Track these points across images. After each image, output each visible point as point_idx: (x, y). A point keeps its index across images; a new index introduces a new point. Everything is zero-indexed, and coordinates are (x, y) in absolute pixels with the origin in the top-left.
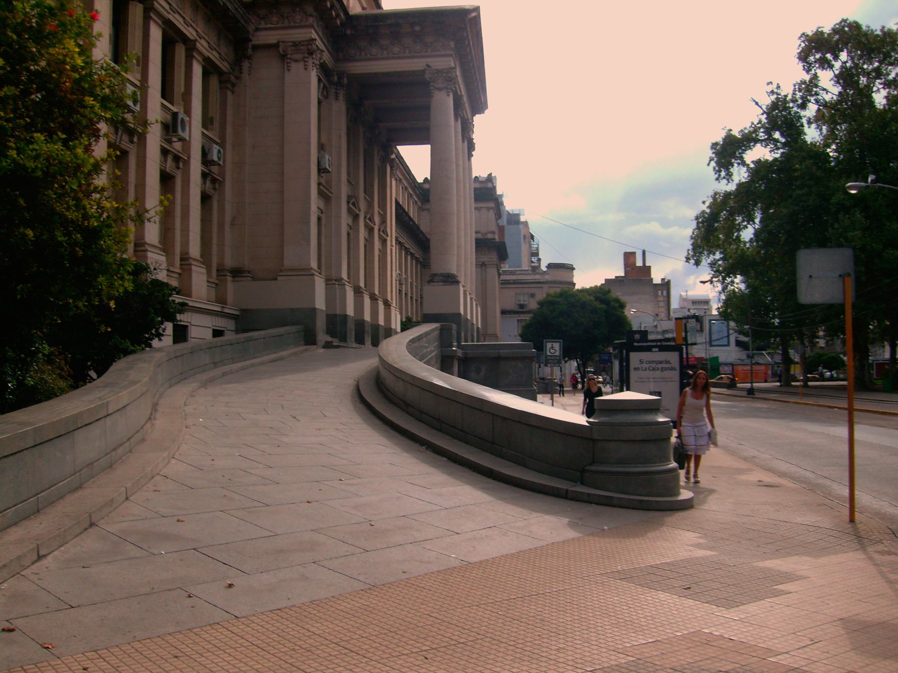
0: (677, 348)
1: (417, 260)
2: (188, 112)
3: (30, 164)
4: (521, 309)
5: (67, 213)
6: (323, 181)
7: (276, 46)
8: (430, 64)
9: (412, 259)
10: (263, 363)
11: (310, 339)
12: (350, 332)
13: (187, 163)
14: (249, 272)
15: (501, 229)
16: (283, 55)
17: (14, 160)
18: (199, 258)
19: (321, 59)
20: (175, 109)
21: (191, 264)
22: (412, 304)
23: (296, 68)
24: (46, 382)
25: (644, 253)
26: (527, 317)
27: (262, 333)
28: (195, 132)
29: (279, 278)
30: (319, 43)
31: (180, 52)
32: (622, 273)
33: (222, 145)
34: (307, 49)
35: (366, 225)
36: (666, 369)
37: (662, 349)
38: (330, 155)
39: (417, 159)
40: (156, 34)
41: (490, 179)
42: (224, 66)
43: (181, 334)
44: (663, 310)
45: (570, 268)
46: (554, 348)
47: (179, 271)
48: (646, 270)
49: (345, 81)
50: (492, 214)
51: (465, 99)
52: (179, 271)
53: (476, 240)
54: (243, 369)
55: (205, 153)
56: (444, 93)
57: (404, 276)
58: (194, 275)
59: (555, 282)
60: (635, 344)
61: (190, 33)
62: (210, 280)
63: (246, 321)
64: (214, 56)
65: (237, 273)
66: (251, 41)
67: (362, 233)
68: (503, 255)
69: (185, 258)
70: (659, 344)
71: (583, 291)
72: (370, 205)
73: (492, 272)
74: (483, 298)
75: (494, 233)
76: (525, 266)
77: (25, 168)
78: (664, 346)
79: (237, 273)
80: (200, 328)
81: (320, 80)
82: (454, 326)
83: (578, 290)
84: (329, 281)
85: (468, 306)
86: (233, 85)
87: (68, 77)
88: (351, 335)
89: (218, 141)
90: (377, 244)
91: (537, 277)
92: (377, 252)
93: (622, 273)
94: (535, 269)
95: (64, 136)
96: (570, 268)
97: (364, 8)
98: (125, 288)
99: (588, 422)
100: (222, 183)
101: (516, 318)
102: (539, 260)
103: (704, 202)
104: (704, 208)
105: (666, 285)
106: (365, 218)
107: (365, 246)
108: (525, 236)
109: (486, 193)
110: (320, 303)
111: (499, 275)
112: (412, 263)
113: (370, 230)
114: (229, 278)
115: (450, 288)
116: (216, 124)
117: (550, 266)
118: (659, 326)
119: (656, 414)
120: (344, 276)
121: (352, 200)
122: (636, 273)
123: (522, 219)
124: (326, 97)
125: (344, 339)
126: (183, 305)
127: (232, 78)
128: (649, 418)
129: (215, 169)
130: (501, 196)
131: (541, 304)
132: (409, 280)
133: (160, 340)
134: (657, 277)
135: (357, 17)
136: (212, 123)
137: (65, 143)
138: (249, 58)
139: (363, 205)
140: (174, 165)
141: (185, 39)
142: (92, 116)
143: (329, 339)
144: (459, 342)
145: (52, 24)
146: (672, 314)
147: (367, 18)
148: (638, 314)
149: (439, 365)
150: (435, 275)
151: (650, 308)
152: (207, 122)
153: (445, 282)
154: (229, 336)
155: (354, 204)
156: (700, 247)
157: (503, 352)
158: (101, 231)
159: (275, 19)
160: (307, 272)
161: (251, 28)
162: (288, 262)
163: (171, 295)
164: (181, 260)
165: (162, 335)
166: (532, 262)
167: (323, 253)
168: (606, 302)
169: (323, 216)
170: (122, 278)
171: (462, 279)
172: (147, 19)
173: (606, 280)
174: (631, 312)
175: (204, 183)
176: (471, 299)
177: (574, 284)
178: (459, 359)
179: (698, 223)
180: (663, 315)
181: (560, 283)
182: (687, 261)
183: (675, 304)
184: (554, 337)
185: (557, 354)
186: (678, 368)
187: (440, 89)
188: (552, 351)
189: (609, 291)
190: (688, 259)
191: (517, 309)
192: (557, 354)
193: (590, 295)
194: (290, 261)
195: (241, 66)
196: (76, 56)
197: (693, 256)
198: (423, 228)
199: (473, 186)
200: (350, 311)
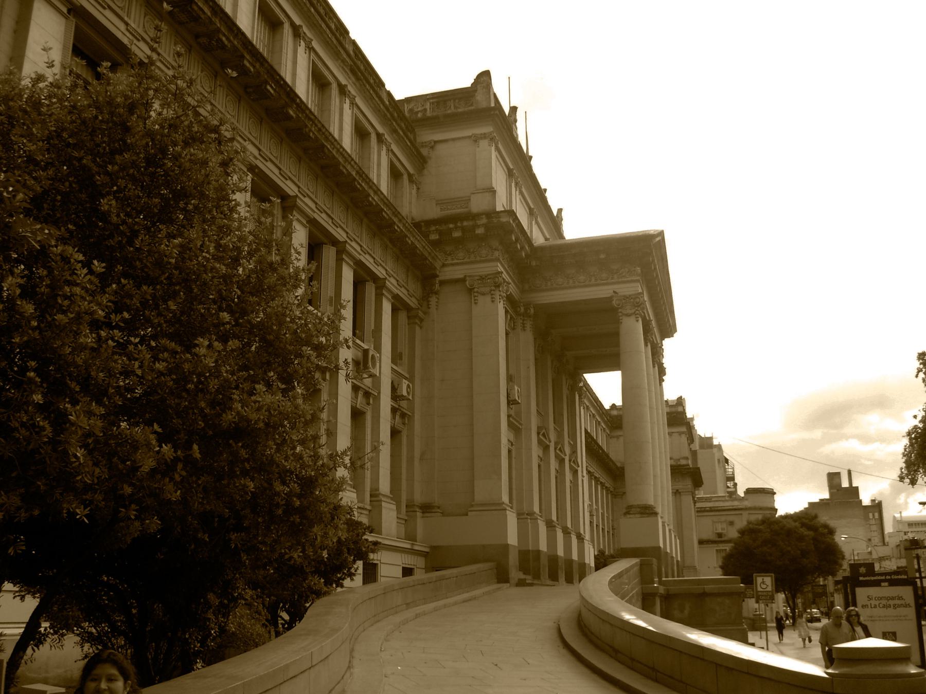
0: (910, 582)
1: (607, 489)
2: (378, 348)
3: (254, 416)
4: (720, 538)
5: (286, 464)
6: (512, 413)
7: (463, 280)
8: (617, 291)
9: (602, 489)
10: (455, 604)
11: (502, 577)
12: (543, 570)
13: (377, 398)
14: (439, 508)
15: (694, 454)
16: (469, 289)
17: (238, 413)
18: (389, 494)
19: (507, 291)
20: (366, 347)
21: (381, 501)
22: (604, 536)
23: (484, 301)
24: (244, 627)
25: (850, 472)
26: (728, 547)
27: (454, 571)
28: (385, 368)
29: (469, 513)
30: (505, 275)
31: (370, 290)
32: (826, 495)
33: (411, 379)
34: (494, 282)
35: (557, 456)
36: (899, 606)
37: (893, 583)
38: (519, 386)
39: (607, 387)
40: (348, 275)
41: (680, 401)
42: (412, 302)
43: (371, 573)
44: (875, 534)
45: (771, 493)
46: (765, 582)
47: (369, 507)
48: (854, 491)
49: (532, 311)
50: (684, 439)
51: (654, 323)
52: (369, 507)
53: (671, 466)
54: (436, 610)
55: (394, 389)
56: (633, 318)
57: (594, 507)
58: (384, 511)
59: (755, 508)
60: (861, 578)
61: (380, 272)
62: (401, 516)
63: (437, 559)
64: (402, 293)
65: (427, 508)
66: (438, 276)
67: (554, 464)
68: (697, 481)
69: (375, 494)
70: (888, 577)
71: (787, 517)
72: (560, 434)
73: (687, 500)
74: (680, 529)
75: (687, 458)
76: (721, 493)
77: (248, 421)
78: (896, 579)
79: (427, 508)
80: (390, 566)
81: (507, 312)
82: (655, 561)
83: (781, 517)
84: (520, 515)
85: (666, 539)
86: (422, 320)
87: (288, 328)
88: (545, 572)
89: (407, 376)
90: (568, 476)
91: (736, 503)
92: (568, 484)
93: (826, 495)
94: (733, 494)
95: (284, 386)
96: (771, 493)
97: (546, 239)
98: (339, 538)
99: (827, 673)
100: (411, 418)
101: (715, 547)
102: (735, 485)
103: (915, 417)
104: (916, 422)
105: (877, 506)
106: (555, 449)
107: (556, 478)
108: (719, 460)
109: (677, 416)
110: (512, 539)
111: (695, 502)
112: (602, 493)
113: (561, 461)
114: (419, 514)
115: (647, 520)
116: (405, 359)
117: (749, 491)
118: (874, 553)
119: (907, 665)
120: (536, 509)
121: (542, 432)
122: (843, 494)
123: (715, 442)
124: (514, 329)
125: (537, 576)
126: (376, 543)
127: (421, 314)
128: (899, 669)
129: (404, 404)
130: (692, 419)
131: (742, 532)
132: (600, 511)
133: (352, 580)
134: (865, 499)
135: (541, 248)
136: (401, 359)
137: (284, 392)
138: (436, 293)
139: (553, 436)
140: (364, 401)
141: (375, 278)
142: (309, 365)
143: (522, 576)
144: (660, 577)
145: (272, 279)
146: (887, 539)
147: (551, 248)
148: (851, 541)
149: (640, 603)
150: (630, 507)
151: (861, 533)
152: (396, 357)
153: (642, 513)
154: (419, 575)
155: (544, 435)
156: (915, 465)
157: (708, 588)
158: (316, 480)
159: (461, 255)
160: (499, 508)
161: (438, 265)
162: (479, 497)
163: (364, 534)
164: (371, 496)
165: (354, 575)
166: (728, 487)
167: (514, 487)
168: (814, 528)
169: (513, 448)
170: (336, 528)
171: (659, 510)
172: (339, 261)
173: (810, 504)
174: (841, 538)
175: (394, 418)
176: (670, 530)
177: (776, 510)
178: (661, 596)
179: (911, 439)
180: (876, 540)
181: (761, 509)
182: (901, 481)
183: (889, 528)
184: (765, 571)
185: (769, 589)
186: (912, 603)
187: (628, 315)
188: (764, 586)
189: (816, 517)
190: (901, 478)
191: (713, 537)
192: (769, 589)
193: (795, 521)
194: (480, 495)
195: (428, 301)
196: (294, 307)
197: (907, 475)
198: (613, 456)
199: (667, 410)
200: (543, 547)
